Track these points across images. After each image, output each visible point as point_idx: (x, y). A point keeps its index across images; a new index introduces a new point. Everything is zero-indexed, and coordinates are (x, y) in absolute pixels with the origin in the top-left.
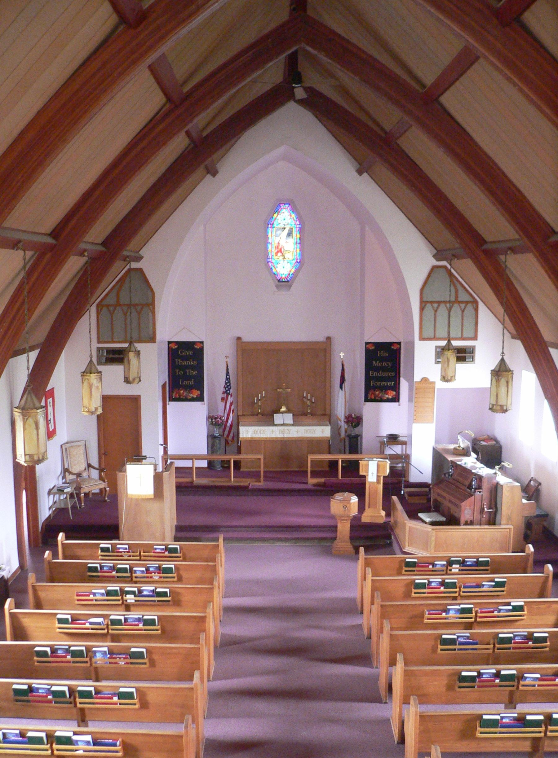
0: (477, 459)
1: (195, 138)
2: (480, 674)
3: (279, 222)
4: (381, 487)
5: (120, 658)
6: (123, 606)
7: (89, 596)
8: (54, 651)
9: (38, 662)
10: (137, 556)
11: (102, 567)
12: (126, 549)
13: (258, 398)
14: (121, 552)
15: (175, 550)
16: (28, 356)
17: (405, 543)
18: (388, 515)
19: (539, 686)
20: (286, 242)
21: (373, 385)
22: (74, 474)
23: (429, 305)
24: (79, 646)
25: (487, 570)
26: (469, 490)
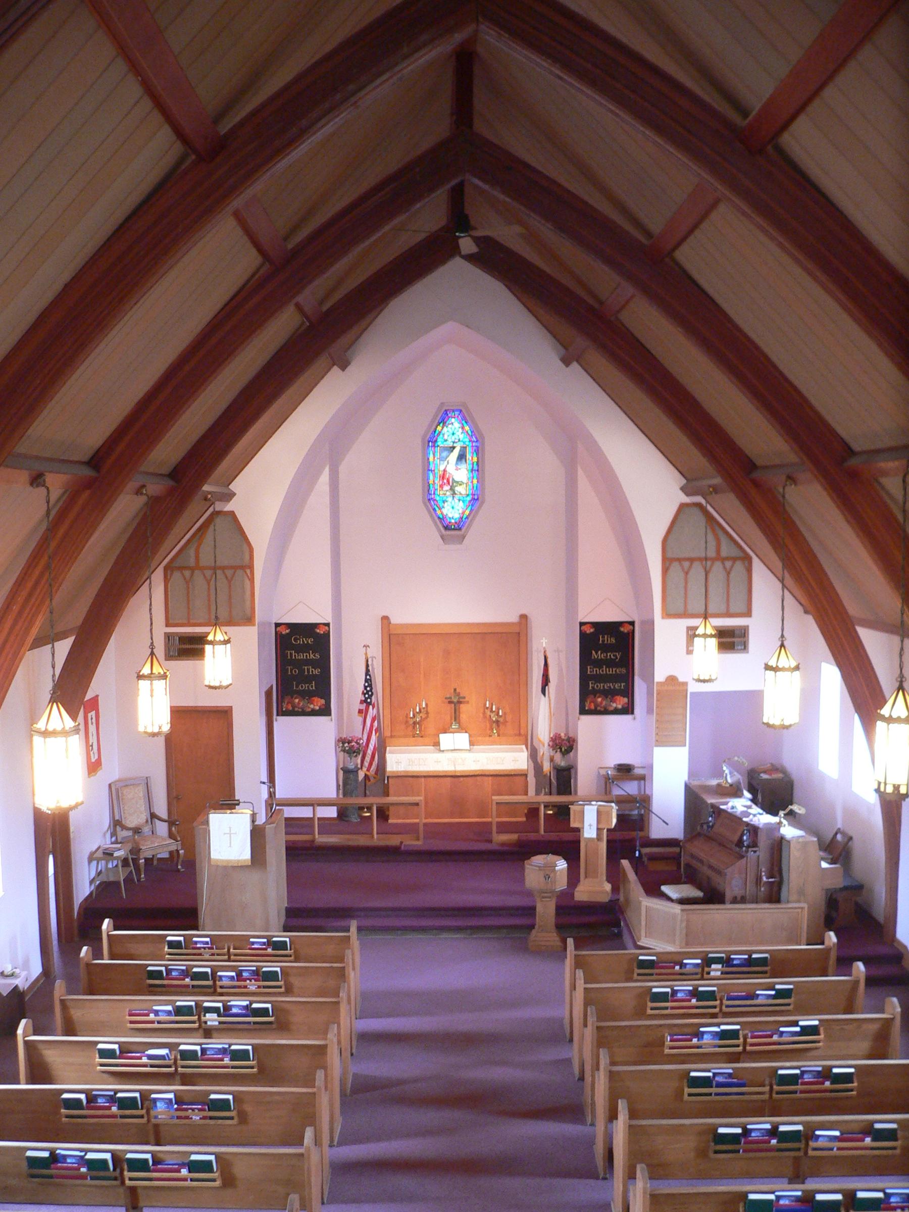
0: (754, 800)
1: (309, 316)
2: (746, 1132)
3: (446, 437)
4: (603, 846)
5: (193, 1110)
6: (201, 1031)
7: (148, 1015)
8: (92, 1098)
9: (67, 1117)
10: (224, 955)
11: (169, 971)
12: (207, 943)
13: (414, 710)
14: (199, 948)
15: (282, 946)
16: (53, 647)
17: (640, 931)
18: (615, 889)
19: (839, 1149)
20: (457, 469)
21: (593, 688)
22: (128, 829)
23: (676, 565)
24: (129, 1091)
25: (766, 972)
26: (738, 849)
